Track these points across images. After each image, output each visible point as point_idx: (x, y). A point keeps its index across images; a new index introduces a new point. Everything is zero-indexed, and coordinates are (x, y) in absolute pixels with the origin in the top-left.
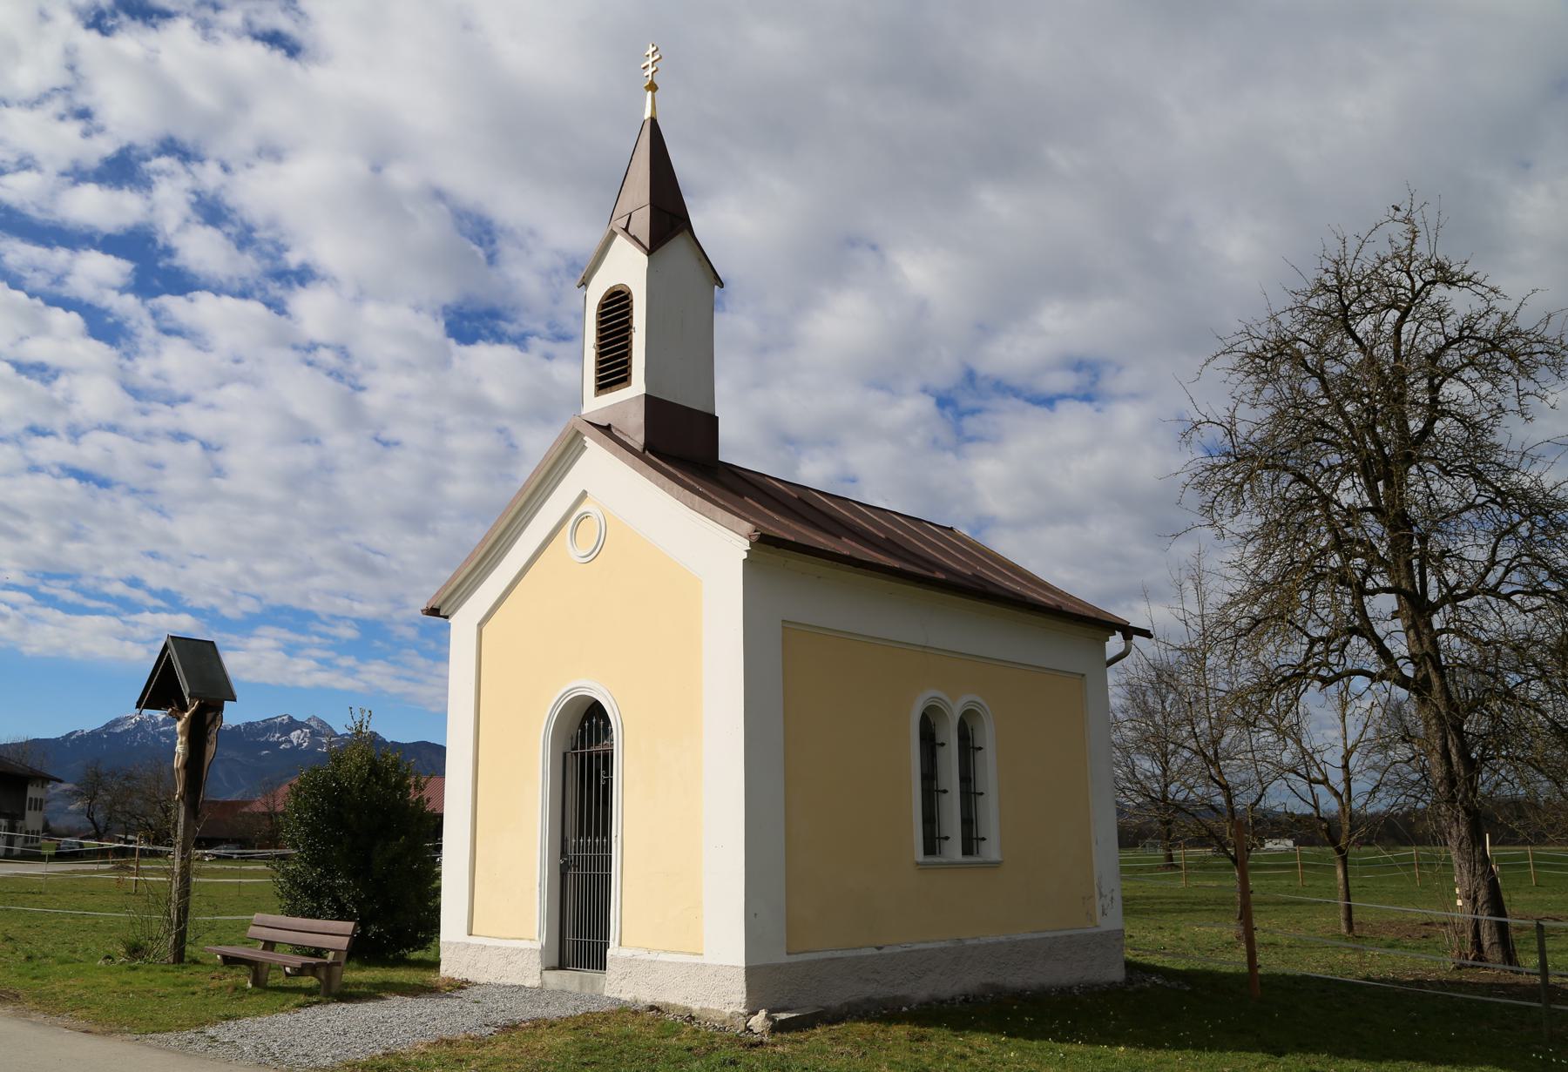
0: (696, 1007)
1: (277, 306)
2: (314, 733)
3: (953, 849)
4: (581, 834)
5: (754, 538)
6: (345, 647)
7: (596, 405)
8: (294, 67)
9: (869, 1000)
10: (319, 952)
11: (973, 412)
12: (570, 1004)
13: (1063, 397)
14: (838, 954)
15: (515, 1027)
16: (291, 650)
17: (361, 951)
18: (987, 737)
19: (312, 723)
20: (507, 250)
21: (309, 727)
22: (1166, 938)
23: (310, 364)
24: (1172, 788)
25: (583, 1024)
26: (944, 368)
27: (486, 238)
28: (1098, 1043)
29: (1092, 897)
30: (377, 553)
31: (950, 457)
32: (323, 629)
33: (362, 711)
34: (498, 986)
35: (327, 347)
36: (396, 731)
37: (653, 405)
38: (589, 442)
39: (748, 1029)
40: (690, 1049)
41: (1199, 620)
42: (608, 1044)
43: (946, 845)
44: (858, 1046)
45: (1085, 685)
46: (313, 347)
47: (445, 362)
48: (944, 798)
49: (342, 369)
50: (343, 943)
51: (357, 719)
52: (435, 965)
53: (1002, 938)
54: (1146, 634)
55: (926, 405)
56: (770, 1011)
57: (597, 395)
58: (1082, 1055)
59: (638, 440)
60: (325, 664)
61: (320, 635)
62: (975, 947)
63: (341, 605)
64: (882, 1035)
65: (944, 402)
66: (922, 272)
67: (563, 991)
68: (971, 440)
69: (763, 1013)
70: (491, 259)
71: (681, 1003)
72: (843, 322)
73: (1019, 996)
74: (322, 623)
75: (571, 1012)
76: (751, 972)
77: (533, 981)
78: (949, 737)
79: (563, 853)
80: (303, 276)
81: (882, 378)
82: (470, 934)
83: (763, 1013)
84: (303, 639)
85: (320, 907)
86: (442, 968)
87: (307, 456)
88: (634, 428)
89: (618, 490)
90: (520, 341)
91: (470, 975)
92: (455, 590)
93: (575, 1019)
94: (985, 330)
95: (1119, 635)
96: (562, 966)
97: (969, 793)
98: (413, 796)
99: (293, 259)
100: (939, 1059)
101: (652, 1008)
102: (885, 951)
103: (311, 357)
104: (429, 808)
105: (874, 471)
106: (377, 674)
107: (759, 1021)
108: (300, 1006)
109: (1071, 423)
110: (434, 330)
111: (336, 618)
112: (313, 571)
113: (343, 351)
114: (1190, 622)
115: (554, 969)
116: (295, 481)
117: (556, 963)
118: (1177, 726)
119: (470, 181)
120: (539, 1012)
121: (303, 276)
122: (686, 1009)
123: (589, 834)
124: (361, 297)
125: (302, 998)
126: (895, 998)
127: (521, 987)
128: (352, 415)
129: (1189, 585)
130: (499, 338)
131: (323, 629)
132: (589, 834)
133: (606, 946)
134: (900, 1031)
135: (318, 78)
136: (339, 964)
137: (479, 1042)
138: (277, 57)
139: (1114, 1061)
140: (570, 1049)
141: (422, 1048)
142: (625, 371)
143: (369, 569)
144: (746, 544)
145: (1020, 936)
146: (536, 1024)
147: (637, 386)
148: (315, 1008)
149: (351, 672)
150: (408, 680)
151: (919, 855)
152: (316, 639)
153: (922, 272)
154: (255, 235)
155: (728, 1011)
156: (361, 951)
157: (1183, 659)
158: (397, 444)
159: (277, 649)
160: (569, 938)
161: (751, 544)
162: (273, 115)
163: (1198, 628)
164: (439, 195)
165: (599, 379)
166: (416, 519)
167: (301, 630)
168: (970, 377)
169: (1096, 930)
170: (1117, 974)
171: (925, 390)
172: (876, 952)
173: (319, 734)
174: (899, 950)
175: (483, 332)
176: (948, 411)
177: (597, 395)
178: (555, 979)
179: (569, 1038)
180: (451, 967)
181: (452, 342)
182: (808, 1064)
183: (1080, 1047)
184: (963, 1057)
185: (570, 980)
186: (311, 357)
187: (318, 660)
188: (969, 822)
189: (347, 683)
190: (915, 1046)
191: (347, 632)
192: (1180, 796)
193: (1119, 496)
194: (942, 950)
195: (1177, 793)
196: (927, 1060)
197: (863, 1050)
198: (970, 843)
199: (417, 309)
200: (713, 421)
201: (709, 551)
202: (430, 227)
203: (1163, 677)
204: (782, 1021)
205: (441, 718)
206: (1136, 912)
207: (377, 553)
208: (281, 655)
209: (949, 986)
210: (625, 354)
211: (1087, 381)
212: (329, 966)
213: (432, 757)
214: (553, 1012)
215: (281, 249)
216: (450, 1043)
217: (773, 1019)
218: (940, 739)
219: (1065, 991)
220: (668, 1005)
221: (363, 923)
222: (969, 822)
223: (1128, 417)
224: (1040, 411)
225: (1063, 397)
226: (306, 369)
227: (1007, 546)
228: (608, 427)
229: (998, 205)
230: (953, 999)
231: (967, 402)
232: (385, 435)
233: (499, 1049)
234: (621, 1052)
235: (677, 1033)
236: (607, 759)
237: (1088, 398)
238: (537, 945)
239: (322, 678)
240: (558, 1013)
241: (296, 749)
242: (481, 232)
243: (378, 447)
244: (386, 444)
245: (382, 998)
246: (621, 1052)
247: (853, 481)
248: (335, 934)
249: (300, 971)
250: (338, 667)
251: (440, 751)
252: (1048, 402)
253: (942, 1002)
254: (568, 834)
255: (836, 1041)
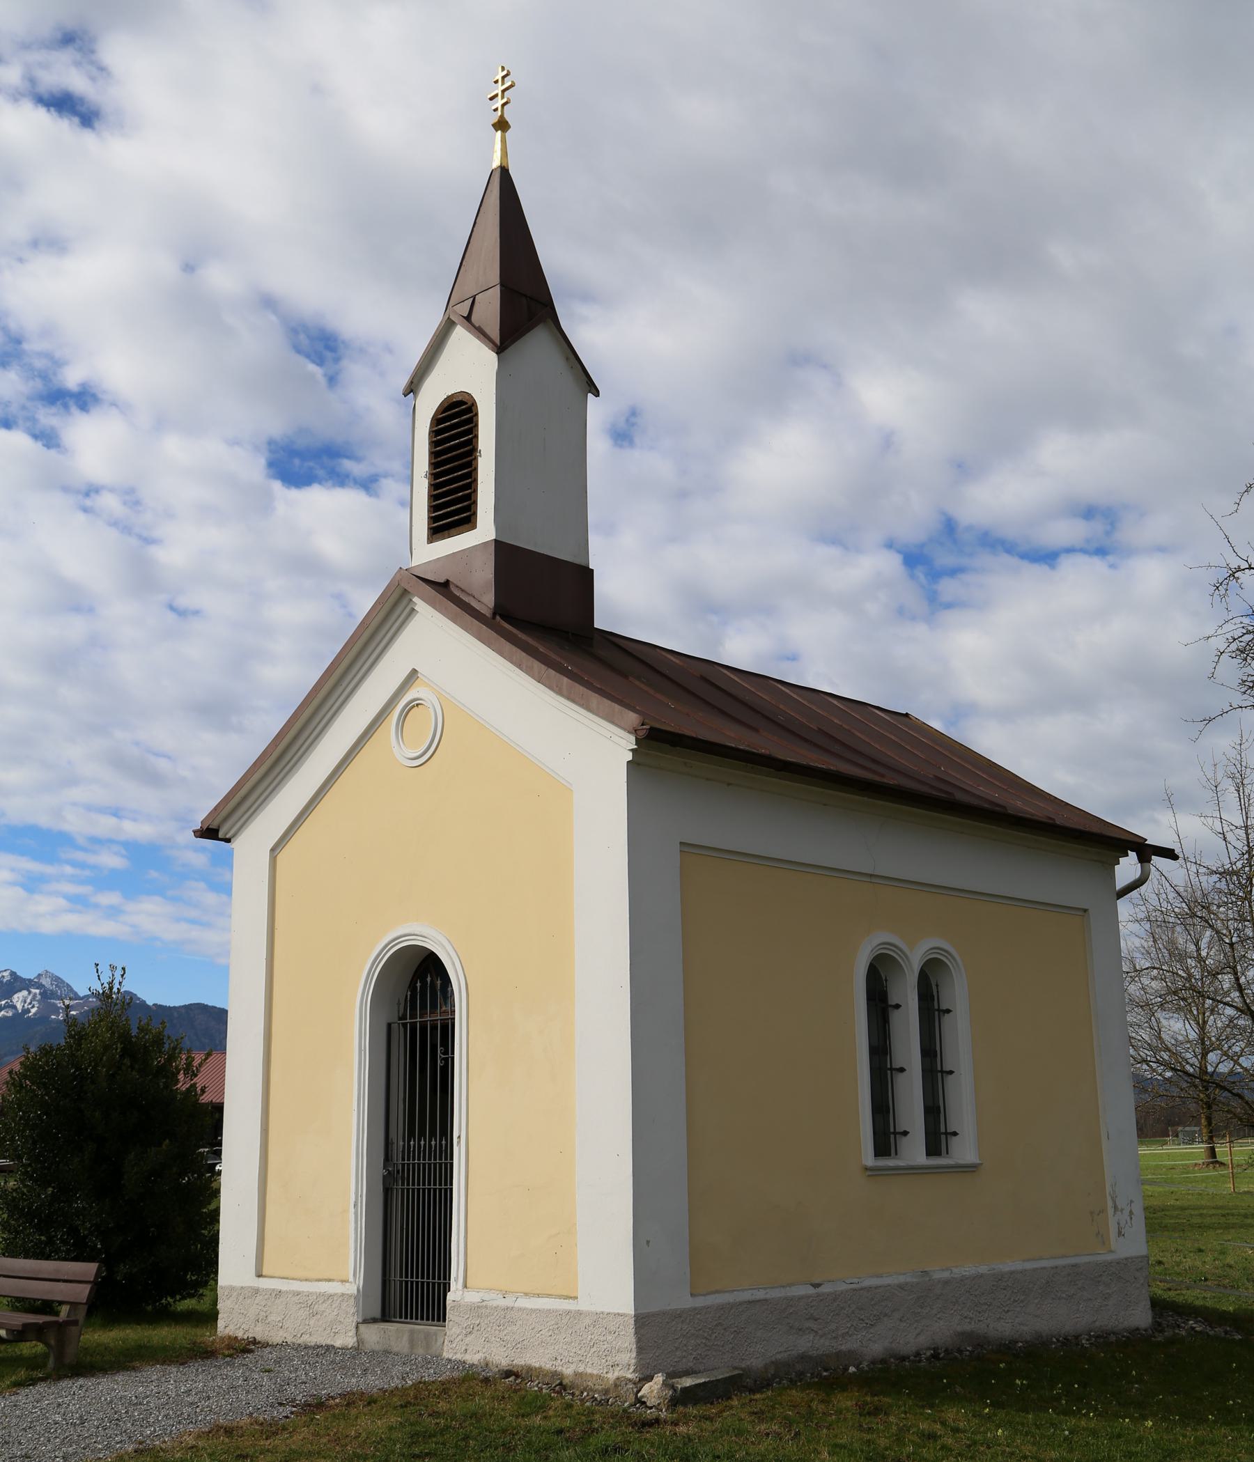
0: (568, 1371)
1: (48, 439)
2: (46, 995)
3: (913, 1150)
4: (411, 1134)
5: (642, 734)
6: (106, 880)
7: (432, 554)
8: (88, 138)
9: (803, 1357)
10: (47, 1307)
11: (954, 572)
12: (397, 1370)
13: (1070, 550)
14: (760, 1295)
15: (320, 1405)
16: (32, 884)
17: (109, 1302)
18: (958, 995)
19: (46, 982)
20: (354, 370)
21: (39, 986)
22: (1207, 1263)
23: (86, 510)
24: (1212, 1057)
25: (412, 1399)
26: (913, 514)
27: (329, 354)
28: (1117, 1416)
29: (1103, 1211)
30: (157, 755)
31: (921, 630)
32: (80, 856)
33: (113, 968)
34: (297, 1348)
35: (112, 490)
36: (158, 989)
37: (504, 552)
38: (420, 605)
39: (640, 1402)
40: (560, 1432)
41: (1242, 833)
42: (447, 1427)
43: (904, 1142)
44: (788, 1423)
45: (1088, 924)
46: (92, 490)
47: (265, 506)
48: (900, 1079)
49: (131, 519)
50: (82, 1293)
51: (106, 979)
52: (211, 1317)
53: (983, 1269)
54: (1169, 854)
55: (891, 563)
56: (670, 1375)
57: (430, 541)
58: (1094, 1433)
59: (487, 600)
60: (79, 903)
61: (74, 864)
62: (946, 1282)
63: (105, 825)
64: (821, 1407)
65: (914, 559)
66: (888, 396)
67: (387, 1352)
68: (949, 606)
69: (659, 1378)
70: (332, 380)
71: (548, 1366)
72: (786, 460)
73: (1007, 1348)
74: (85, 850)
75: (396, 1382)
76: (642, 1321)
77: (346, 1339)
78: (906, 996)
79: (387, 1159)
80: (84, 399)
81: (835, 533)
82: (259, 1275)
83: (659, 1378)
84: (48, 869)
85: (50, 1241)
86: (221, 1323)
87: (75, 629)
88: (481, 583)
89: (449, 659)
90: (368, 484)
91: (259, 1332)
92: (239, 804)
93: (404, 1391)
94: (963, 469)
95: (1133, 855)
96: (385, 1317)
97: (934, 1072)
98: (183, 1084)
99: (72, 378)
100: (899, 1440)
101: (508, 1373)
102: (822, 1290)
103: (88, 503)
104: (205, 1099)
105: (822, 644)
106: (149, 916)
107: (653, 1390)
108: (19, 1384)
109: (1078, 583)
110: (253, 468)
111: (98, 842)
112: (72, 781)
113: (131, 497)
114: (1229, 836)
115: (374, 1321)
116: (59, 662)
117: (378, 1314)
118: (1214, 975)
119: (314, 288)
120: (353, 1383)
121: (84, 399)
122: (555, 1374)
123: (422, 1134)
124: (162, 423)
125: (22, 1374)
126: (838, 1354)
127: (329, 1348)
128: (142, 577)
129: (1229, 787)
130: (340, 479)
131: (80, 856)
132: (422, 1134)
133: (446, 1288)
134: (846, 1401)
135: (112, 151)
136: (75, 1323)
137: (271, 1429)
138: (62, 128)
139: (1139, 1440)
140: (395, 1435)
141: (190, 1441)
142: (468, 509)
143: (153, 778)
144: (629, 742)
145: (1007, 1266)
146: (350, 1399)
147: (485, 529)
148: (41, 1387)
149: (113, 912)
150: (193, 922)
151: (869, 1159)
152: (68, 870)
153: (888, 396)
154: (26, 346)
155: (612, 1376)
156: (109, 1302)
157: (1223, 885)
158: (196, 613)
159: (13, 884)
160: (396, 1277)
161: (638, 742)
162: (56, 196)
163: (1239, 845)
164: (268, 302)
165: (432, 520)
166: (215, 711)
167: (51, 859)
168: (950, 527)
169: (1109, 1257)
170: (1141, 1317)
171: (890, 545)
172: (811, 1291)
173: (53, 995)
174: (843, 1287)
175: (321, 473)
176: (920, 572)
177: (430, 541)
178: (375, 1335)
179: (394, 1420)
180: (232, 1320)
181: (277, 486)
182: (721, 1449)
183: (1090, 1421)
184: (932, 1436)
185: (397, 1335)
186: (88, 503)
187: (69, 898)
188: (934, 1110)
189: (106, 928)
190: (866, 1422)
191: (111, 860)
192: (1224, 1068)
193: (1138, 676)
194: (901, 1287)
195: (1217, 1063)
196: (883, 1442)
197: (795, 1428)
198: (936, 1140)
199: (234, 442)
200: (585, 576)
201: (588, 751)
202: (258, 343)
203: (1197, 910)
204: (685, 1390)
205: (223, 972)
206: (1165, 1228)
207: (157, 755)
208: (20, 892)
209: (914, 1336)
210: (468, 486)
211: (1102, 530)
212: (61, 1327)
213: (210, 1024)
214: (373, 1382)
215: (58, 364)
216: (229, 1431)
217: (673, 1387)
218: (893, 1000)
219: (1069, 1341)
220: (530, 1369)
221: (109, 1262)
222: (934, 1110)
223: (1152, 576)
224: (1039, 570)
225: (1070, 550)
226: (81, 517)
227: (994, 743)
228: (446, 584)
229: (986, 314)
230: (918, 1354)
231: (945, 559)
232: (183, 601)
233: (297, 1437)
234: (466, 1438)
235: (543, 1408)
236: (446, 1031)
237: (1101, 552)
238: (351, 1289)
239: (72, 921)
240: (380, 1384)
241: (20, 1017)
242: (321, 346)
243: (171, 616)
244: (182, 613)
245: (134, 1369)
246: (466, 1438)
247: (793, 658)
248: (68, 1279)
249: (20, 1335)
250: (96, 906)
251: (220, 1016)
252: (1047, 557)
253: (903, 1358)
254: (393, 1135)
255: (759, 1416)
